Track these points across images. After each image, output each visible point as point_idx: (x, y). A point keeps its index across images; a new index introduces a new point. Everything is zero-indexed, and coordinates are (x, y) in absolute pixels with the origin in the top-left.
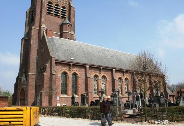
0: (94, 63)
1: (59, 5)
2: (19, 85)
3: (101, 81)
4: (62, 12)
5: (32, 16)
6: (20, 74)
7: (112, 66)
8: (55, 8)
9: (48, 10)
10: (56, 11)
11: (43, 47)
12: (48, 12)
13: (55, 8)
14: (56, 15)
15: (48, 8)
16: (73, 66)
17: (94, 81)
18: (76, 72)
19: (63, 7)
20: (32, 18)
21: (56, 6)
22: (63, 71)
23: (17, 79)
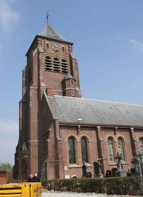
1: (58, 58)
3: (117, 144)
5: (30, 75)
7: (129, 124)
8: (54, 63)
9: (46, 66)
10: (56, 66)
12: (46, 69)
13: (54, 63)
14: (56, 71)
15: (46, 63)
18: (86, 135)
19: (64, 61)
21: (55, 60)
22: (70, 135)
23: (17, 148)
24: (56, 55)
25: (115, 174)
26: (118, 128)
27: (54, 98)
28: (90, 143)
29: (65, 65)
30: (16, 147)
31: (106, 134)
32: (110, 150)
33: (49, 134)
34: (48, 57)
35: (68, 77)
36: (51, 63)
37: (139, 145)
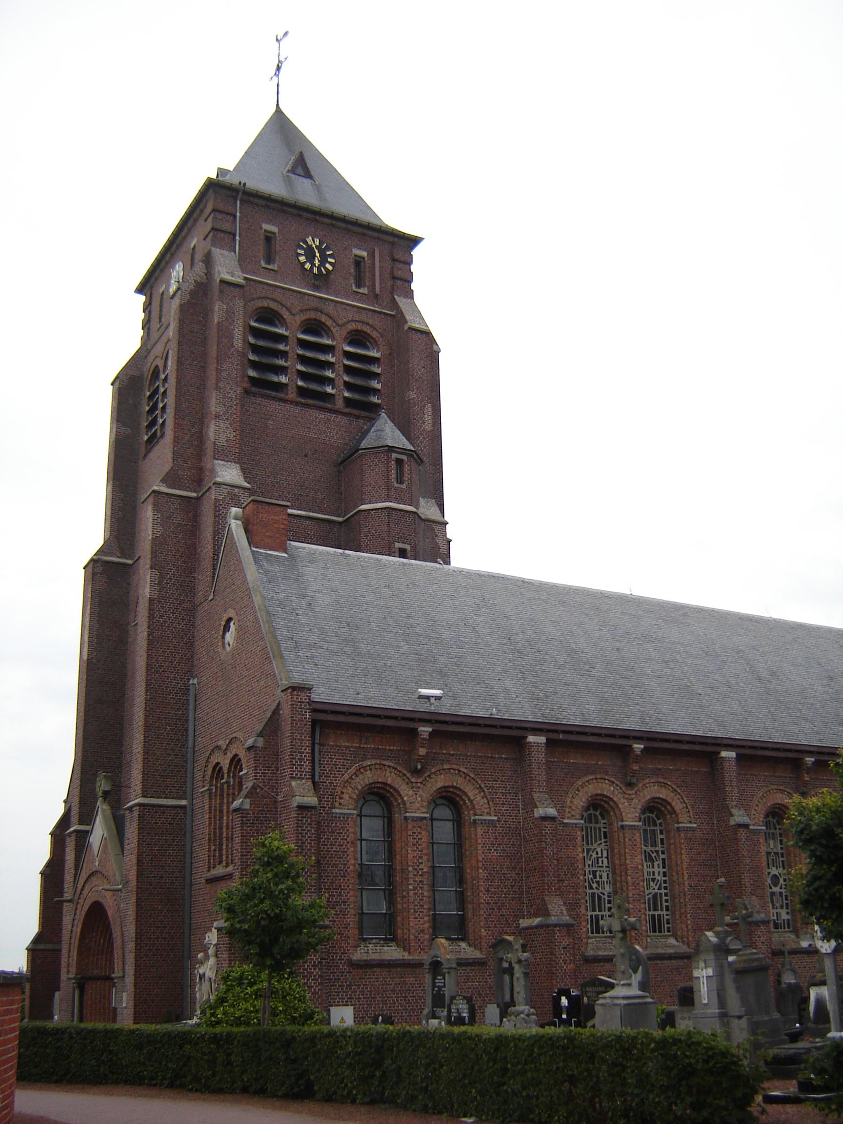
1: (329, 323)
2: (76, 876)
3: (638, 837)
4: (348, 370)
5: (154, 408)
6: (76, 800)
7: (718, 732)
8: (300, 352)
9: (254, 365)
10: (311, 370)
11: (230, 620)
13: (300, 352)
14: (313, 397)
15: (255, 349)
17: (587, 840)
18: (459, 782)
19: (358, 338)
20: (153, 423)
21: (305, 332)
22: (368, 777)
23: (59, 835)
24: (314, 303)
25: (597, 1008)
26: (645, 750)
27: (292, 558)
28: (480, 831)
30: (51, 829)
31: (580, 783)
32: (594, 873)
33: (403, 317)
34: (268, 316)
35: (379, 438)
36: (281, 347)
37: (763, 849)
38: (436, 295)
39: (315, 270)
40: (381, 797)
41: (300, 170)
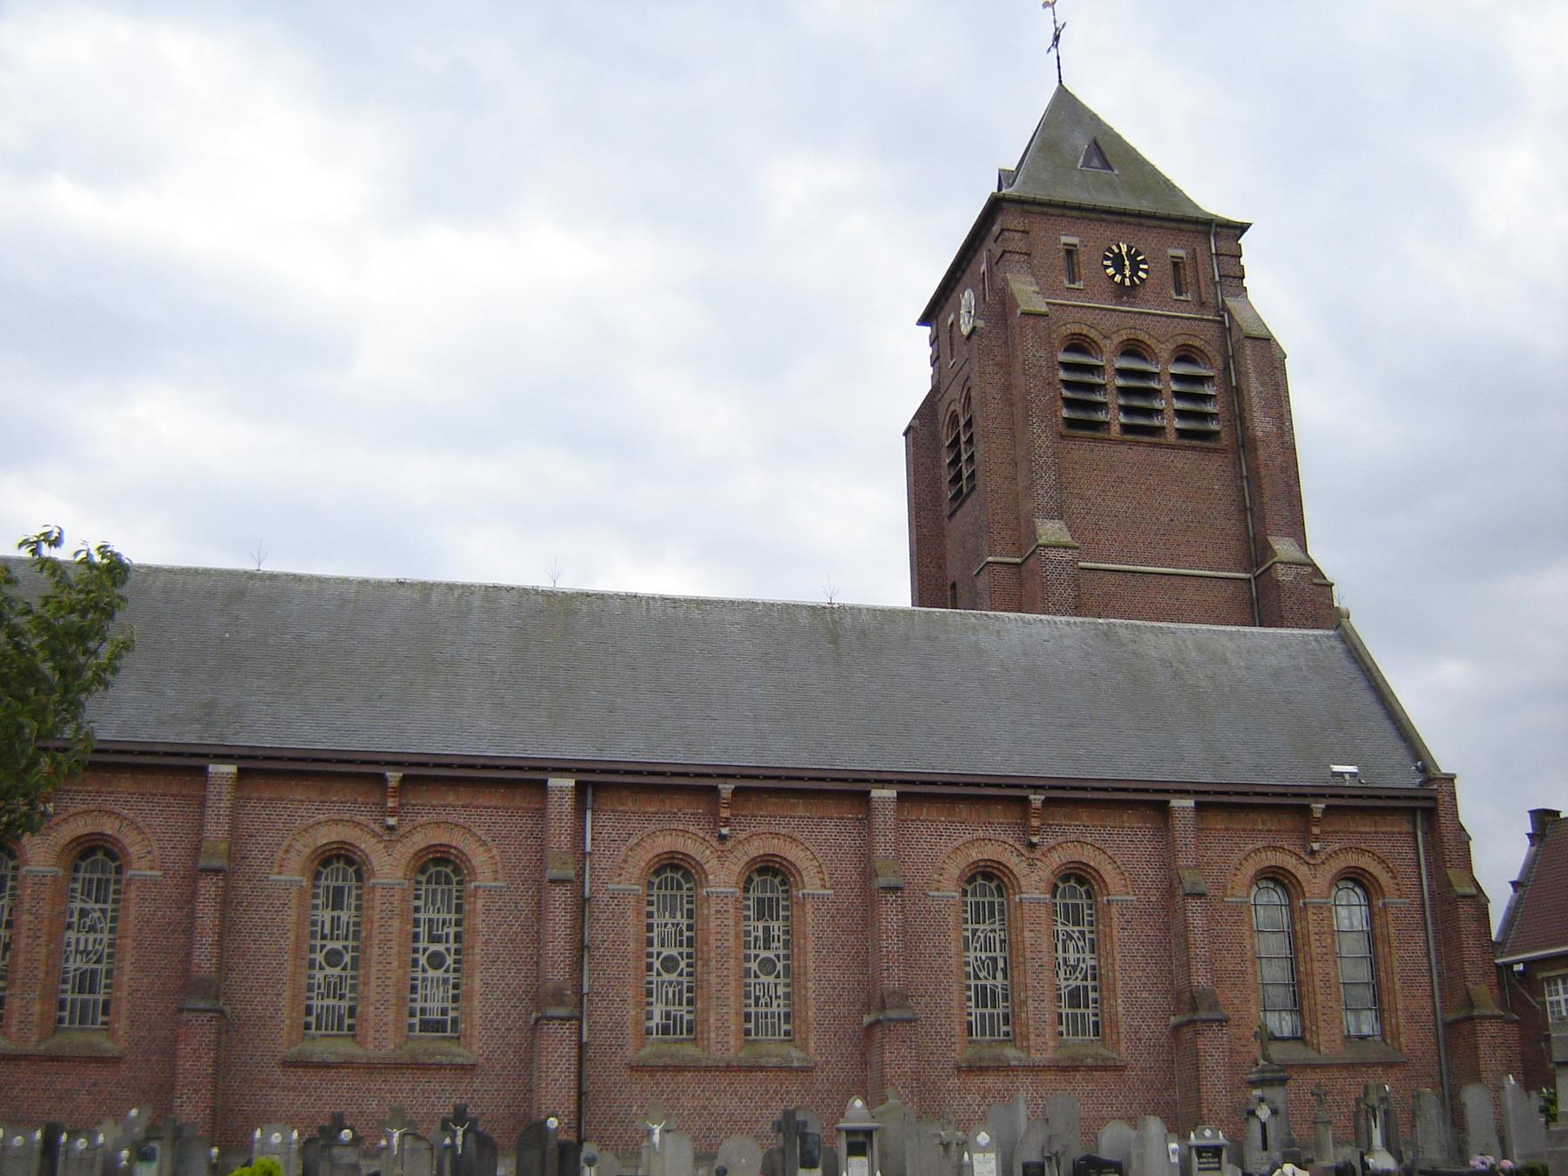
0: (1242, 767)
7: (1163, 774)
9: (1069, 403)
12: (1070, 423)
14: (1142, 431)
16: (1219, 823)
19: (1185, 355)
29: (1144, 385)
34: (1078, 344)
38: (1271, 292)
39: (1127, 282)
40: (674, 869)
41: (1095, 162)
